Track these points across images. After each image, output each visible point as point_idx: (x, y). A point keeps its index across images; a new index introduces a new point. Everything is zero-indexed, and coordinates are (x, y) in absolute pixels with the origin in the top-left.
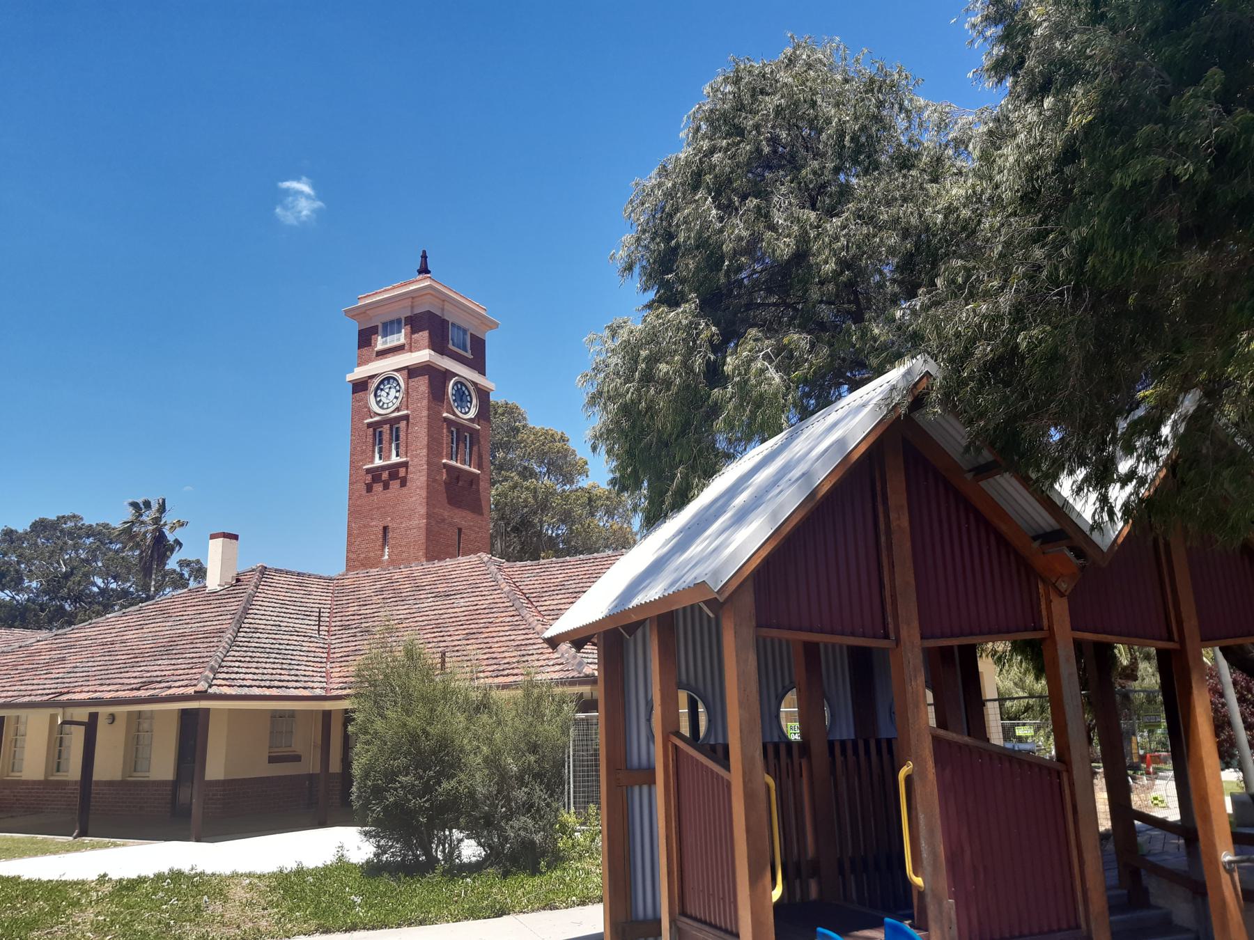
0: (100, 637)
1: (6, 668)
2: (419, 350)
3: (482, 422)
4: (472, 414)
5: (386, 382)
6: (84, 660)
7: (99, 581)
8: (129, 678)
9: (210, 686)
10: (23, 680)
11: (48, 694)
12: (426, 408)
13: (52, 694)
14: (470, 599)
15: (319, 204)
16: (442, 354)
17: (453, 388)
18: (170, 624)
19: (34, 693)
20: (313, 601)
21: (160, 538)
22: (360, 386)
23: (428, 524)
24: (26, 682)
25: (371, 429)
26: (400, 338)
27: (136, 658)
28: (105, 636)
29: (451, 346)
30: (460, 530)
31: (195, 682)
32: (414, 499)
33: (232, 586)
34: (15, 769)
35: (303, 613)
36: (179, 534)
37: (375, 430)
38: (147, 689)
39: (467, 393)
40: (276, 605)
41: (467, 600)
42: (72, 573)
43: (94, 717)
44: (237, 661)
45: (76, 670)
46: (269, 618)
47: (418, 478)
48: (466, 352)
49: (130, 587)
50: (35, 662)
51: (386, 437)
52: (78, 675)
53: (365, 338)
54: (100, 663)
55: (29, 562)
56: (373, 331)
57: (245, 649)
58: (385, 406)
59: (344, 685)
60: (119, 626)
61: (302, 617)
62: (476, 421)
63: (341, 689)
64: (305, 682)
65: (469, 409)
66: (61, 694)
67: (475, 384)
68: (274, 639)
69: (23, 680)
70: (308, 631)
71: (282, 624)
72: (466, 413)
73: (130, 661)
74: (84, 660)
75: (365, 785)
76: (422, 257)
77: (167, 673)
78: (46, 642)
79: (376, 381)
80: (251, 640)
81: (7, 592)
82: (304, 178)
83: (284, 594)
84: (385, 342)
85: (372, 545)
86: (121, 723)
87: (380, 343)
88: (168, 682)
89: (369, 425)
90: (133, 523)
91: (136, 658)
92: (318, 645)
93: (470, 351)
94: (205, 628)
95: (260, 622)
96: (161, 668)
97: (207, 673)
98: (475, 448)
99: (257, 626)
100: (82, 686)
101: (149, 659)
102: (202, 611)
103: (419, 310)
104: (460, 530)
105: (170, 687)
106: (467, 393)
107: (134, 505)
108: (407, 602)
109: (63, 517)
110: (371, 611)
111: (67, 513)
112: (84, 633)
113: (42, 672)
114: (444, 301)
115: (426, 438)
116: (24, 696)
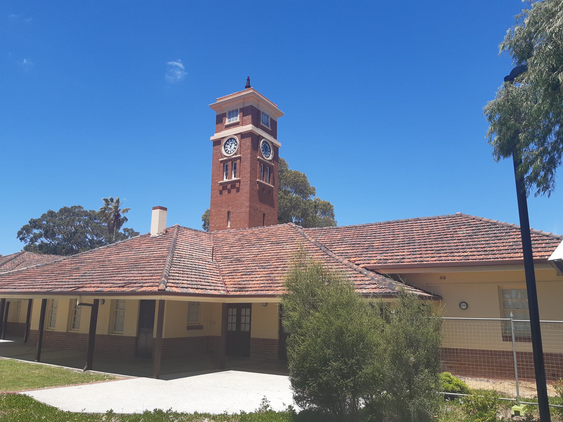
0: (97, 258)
1: (48, 272)
2: (247, 125)
3: (275, 162)
4: (270, 158)
5: (230, 141)
6: (90, 269)
7: (89, 237)
8: (117, 280)
9: (166, 287)
10: (57, 279)
11: (71, 288)
12: (250, 153)
13: (73, 287)
14: (293, 245)
15: (186, 73)
16: (257, 127)
17: (262, 144)
18: (133, 252)
19: (63, 286)
20: (204, 244)
21: (117, 216)
22: (217, 143)
23: (250, 211)
24: (59, 280)
25: (222, 164)
26: (237, 119)
27: (119, 270)
28: (100, 258)
29: (261, 124)
30: (264, 214)
31: (158, 284)
32: (243, 198)
33: (164, 234)
34: (51, 326)
35: (202, 249)
36: (126, 215)
37: (224, 164)
38: (128, 287)
39: (268, 148)
40: (188, 245)
41: (291, 246)
42: (76, 232)
43: (96, 301)
44: (176, 273)
45: (86, 275)
46: (186, 251)
47: (245, 188)
48: (268, 127)
49: (102, 239)
50: (63, 270)
51: (230, 167)
52: (87, 277)
53: (220, 119)
54: (99, 271)
55: (59, 225)
56: (224, 115)
57: (178, 266)
58: (229, 152)
59: (236, 289)
60: (106, 253)
61: (202, 251)
62: (272, 161)
63: (235, 291)
64: (214, 286)
65: (269, 155)
66: (79, 288)
67: (272, 143)
68: (192, 262)
69: (57, 279)
70: (206, 259)
71: (193, 254)
72: (268, 157)
73: (116, 271)
74: (90, 269)
75: (303, 366)
76: (247, 80)
77: (138, 278)
78: (68, 260)
79: (225, 140)
80: (181, 262)
81: (48, 239)
82: (180, 60)
83: (190, 239)
84: (230, 121)
85: (222, 220)
86: (108, 305)
87: (227, 122)
88: (140, 283)
89: (221, 162)
90: (105, 209)
91: (119, 270)
92: (213, 266)
93: (270, 127)
94: (154, 255)
95: (182, 253)
96: (134, 275)
97: (163, 279)
98: (272, 175)
99: (181, 255)
100: (90, 283)
101: (126, 270)
102: (150, 246)
103: (247, 105)
104: (264, 214)
105: (142, 287)
106: (268, 148)
107: (106, 200)
108: (256, 246)
109: (75, 206)
110: (237, 250)
111: (77, 205)
112: (87, 255)
113: (67, 275)
114: (259, 100)
115: (249, 168)
116: (58, 288)
